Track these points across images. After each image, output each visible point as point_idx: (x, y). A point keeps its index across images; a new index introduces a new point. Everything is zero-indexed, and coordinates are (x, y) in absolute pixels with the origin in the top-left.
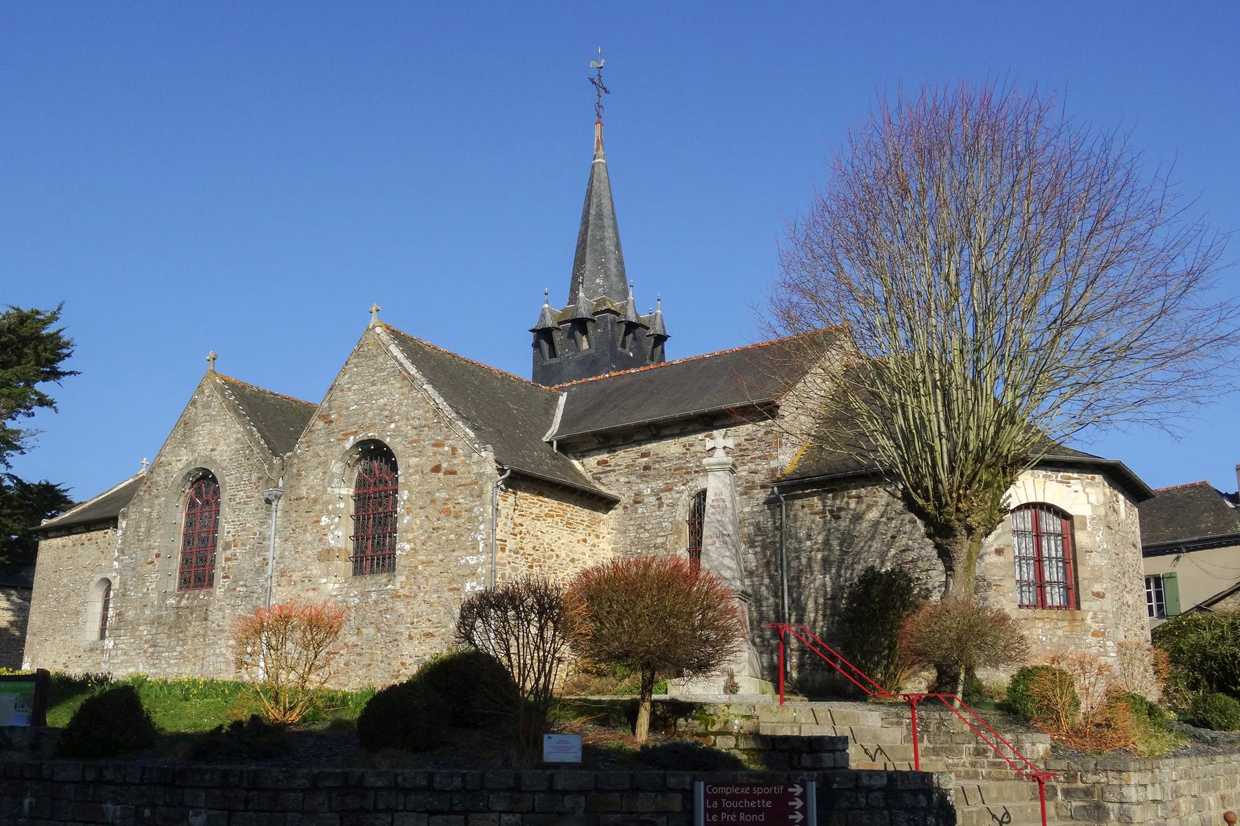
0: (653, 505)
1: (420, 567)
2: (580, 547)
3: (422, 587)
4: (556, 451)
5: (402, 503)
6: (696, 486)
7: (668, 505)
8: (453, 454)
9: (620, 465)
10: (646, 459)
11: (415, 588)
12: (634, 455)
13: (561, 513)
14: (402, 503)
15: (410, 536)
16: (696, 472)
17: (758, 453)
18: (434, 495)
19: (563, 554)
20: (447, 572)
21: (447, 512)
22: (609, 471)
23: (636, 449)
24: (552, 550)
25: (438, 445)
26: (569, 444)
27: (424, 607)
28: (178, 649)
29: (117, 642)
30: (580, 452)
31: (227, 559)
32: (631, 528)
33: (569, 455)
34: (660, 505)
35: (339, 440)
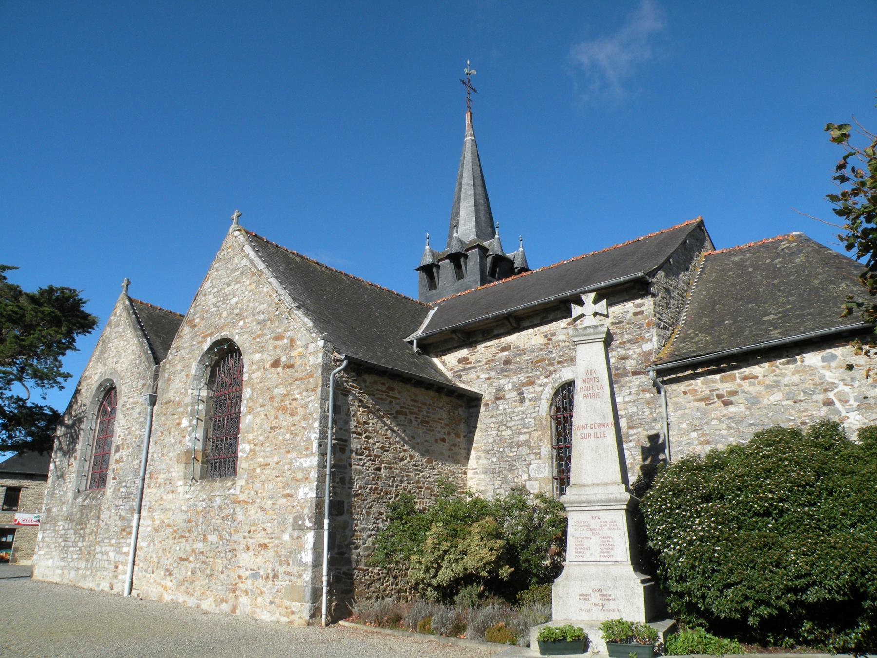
0: (515, 401)
1: (258, 470)
3: (259, 492)
5: (245, 402)
6: (560, 378)
7: (530, 400)
8: (292, 346)
9: (480, 361)
10: (506, 353)
11: (253, 493)
12: (493, 350)
13: (416, 410)
14: (245, 402)
15: (251, 436)
16: (559, 362)
17: (626, 337)
18: (273, 392)
20: (282, 476)
21: (284, 409)
22: (470, 369)
23: (495, 342)
25: (279, 337)
26: (430, 344)
27: (260, 514)
28: (80, 544)
29: (45, 535)
30: (441, 352)
31: (117, 461)
32: (492, 426)
33: (431, 355)
35: (199, 343)
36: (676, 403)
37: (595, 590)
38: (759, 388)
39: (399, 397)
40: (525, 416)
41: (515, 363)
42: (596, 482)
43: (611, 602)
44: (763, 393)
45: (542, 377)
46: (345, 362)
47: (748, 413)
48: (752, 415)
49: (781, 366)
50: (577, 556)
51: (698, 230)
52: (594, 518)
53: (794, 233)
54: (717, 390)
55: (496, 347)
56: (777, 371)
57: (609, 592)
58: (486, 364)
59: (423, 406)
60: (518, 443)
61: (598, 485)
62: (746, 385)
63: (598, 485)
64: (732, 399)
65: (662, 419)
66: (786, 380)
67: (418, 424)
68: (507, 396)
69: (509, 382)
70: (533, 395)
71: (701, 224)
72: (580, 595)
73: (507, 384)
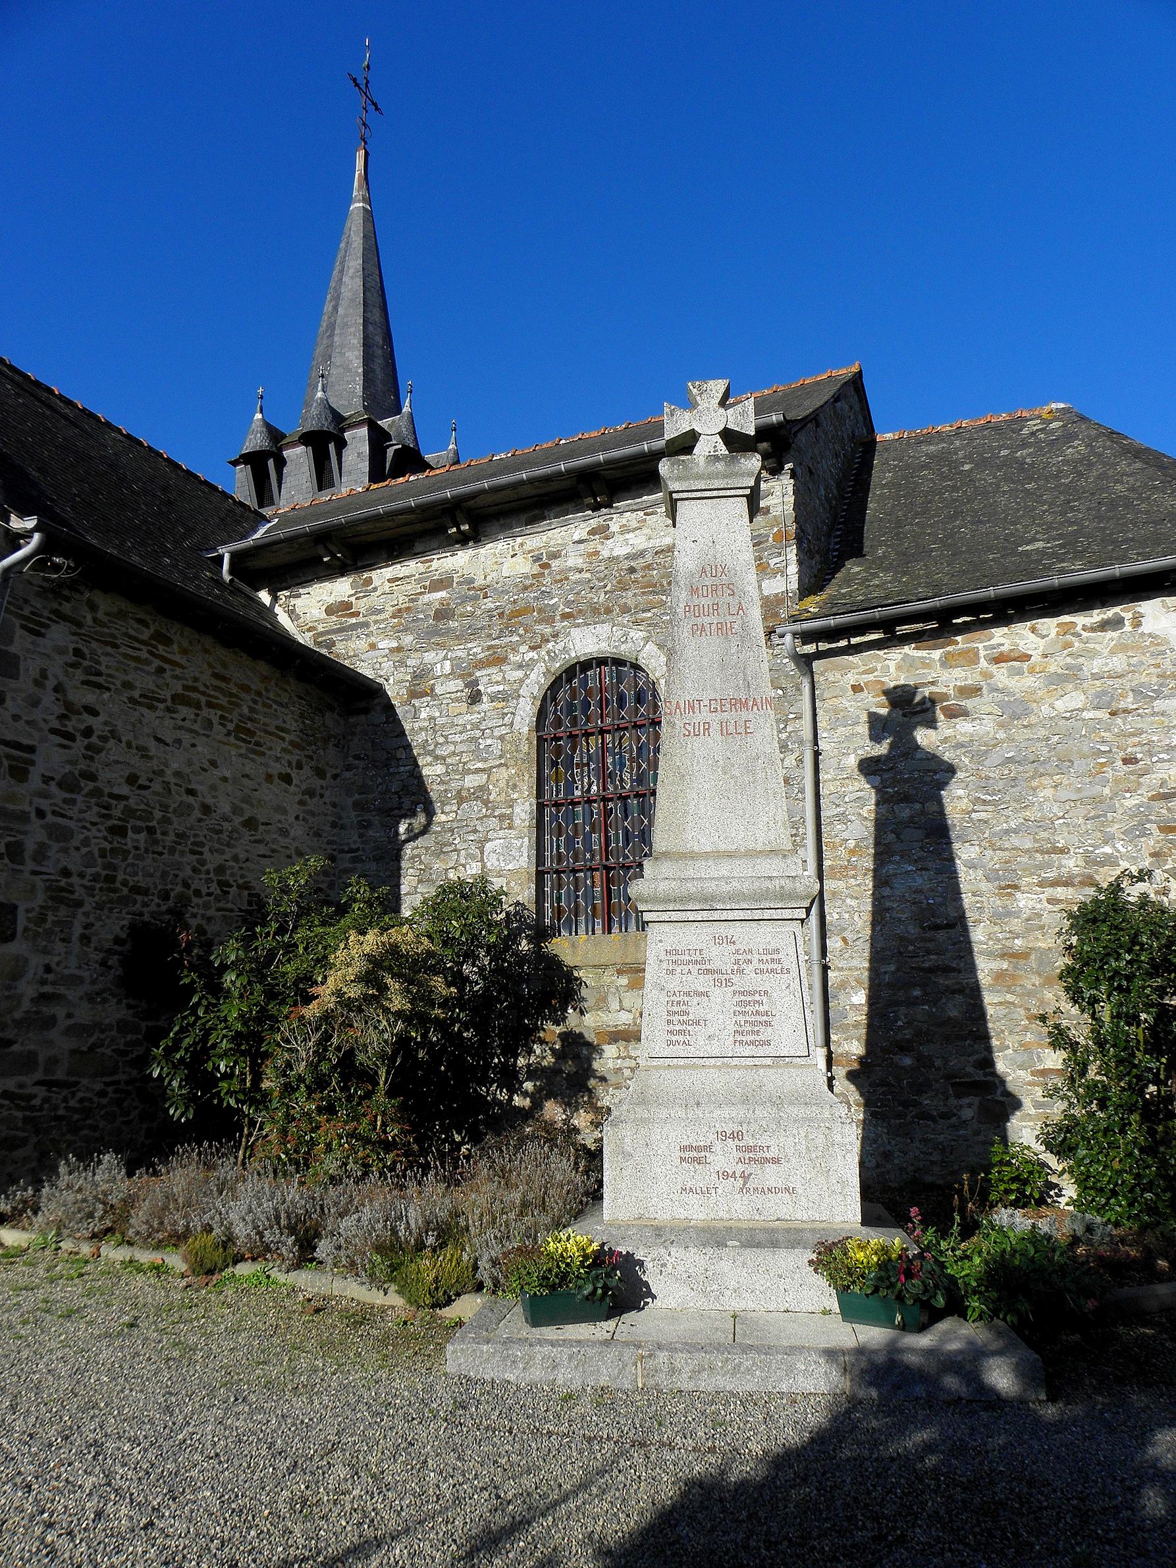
0: (458, 700)
2: (271, 794)
4: (227, 577)
6: (565, 650)
9: (380, 611)
10: (442, 594)
13: (223, 701)
16: (565, 616)
19: (225, 808)
22: (354, 627)
23: (412, 567)
24: (191, 792)
34: (475, 698)
36: (836, 711)
37: (723, 1136)
38: (1029, 681)
39: (183, 662)
40: (478, 733)
41: (462, 615)
42: (722, 847)
43: (770, 1168)
44: (1040, 693)
45: (523, 648)
46: (37, 537)
47: (1001, 735)
48: (1011, 739)
49: (1085, 634)
50: (670, 1043)
51: (851, 391)
52: (718, 940)
53: (1054, 406)
54: (932, 683)
55: (418, 581)
56: (1077, 644)
57: (763, 1141)
58: (393, 617)
59: (243, 695)
60: (459, 792)
61: (730, 855)
62: (1001, 675)
63: (730, 855)
64: (969, 704)
65: (801, 742)
66: (1096, 665)
67: (228, 734)
68: (439, 690)
69: (445, 658)
70: (501, 688)
71: (856, 383)
72: (684, 1149)
73: (439, 662)
